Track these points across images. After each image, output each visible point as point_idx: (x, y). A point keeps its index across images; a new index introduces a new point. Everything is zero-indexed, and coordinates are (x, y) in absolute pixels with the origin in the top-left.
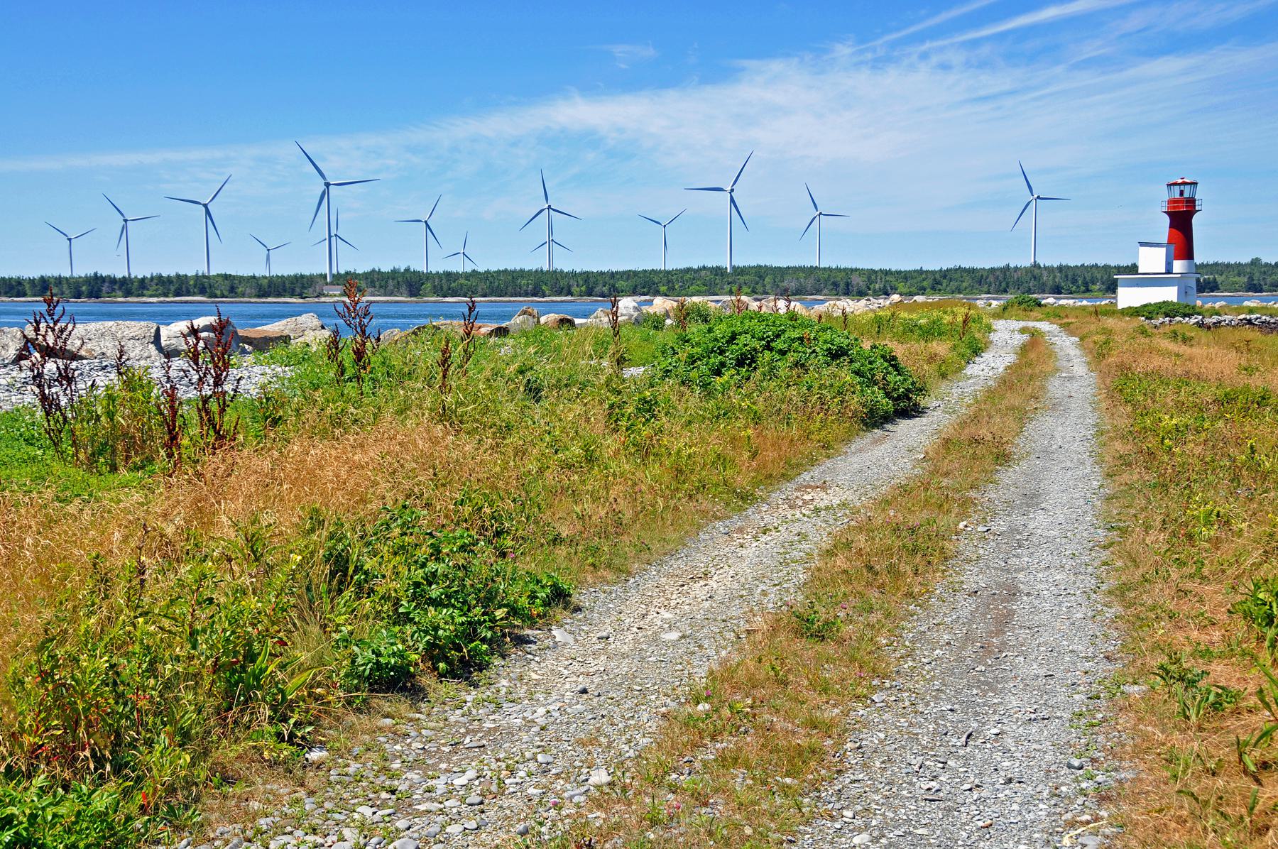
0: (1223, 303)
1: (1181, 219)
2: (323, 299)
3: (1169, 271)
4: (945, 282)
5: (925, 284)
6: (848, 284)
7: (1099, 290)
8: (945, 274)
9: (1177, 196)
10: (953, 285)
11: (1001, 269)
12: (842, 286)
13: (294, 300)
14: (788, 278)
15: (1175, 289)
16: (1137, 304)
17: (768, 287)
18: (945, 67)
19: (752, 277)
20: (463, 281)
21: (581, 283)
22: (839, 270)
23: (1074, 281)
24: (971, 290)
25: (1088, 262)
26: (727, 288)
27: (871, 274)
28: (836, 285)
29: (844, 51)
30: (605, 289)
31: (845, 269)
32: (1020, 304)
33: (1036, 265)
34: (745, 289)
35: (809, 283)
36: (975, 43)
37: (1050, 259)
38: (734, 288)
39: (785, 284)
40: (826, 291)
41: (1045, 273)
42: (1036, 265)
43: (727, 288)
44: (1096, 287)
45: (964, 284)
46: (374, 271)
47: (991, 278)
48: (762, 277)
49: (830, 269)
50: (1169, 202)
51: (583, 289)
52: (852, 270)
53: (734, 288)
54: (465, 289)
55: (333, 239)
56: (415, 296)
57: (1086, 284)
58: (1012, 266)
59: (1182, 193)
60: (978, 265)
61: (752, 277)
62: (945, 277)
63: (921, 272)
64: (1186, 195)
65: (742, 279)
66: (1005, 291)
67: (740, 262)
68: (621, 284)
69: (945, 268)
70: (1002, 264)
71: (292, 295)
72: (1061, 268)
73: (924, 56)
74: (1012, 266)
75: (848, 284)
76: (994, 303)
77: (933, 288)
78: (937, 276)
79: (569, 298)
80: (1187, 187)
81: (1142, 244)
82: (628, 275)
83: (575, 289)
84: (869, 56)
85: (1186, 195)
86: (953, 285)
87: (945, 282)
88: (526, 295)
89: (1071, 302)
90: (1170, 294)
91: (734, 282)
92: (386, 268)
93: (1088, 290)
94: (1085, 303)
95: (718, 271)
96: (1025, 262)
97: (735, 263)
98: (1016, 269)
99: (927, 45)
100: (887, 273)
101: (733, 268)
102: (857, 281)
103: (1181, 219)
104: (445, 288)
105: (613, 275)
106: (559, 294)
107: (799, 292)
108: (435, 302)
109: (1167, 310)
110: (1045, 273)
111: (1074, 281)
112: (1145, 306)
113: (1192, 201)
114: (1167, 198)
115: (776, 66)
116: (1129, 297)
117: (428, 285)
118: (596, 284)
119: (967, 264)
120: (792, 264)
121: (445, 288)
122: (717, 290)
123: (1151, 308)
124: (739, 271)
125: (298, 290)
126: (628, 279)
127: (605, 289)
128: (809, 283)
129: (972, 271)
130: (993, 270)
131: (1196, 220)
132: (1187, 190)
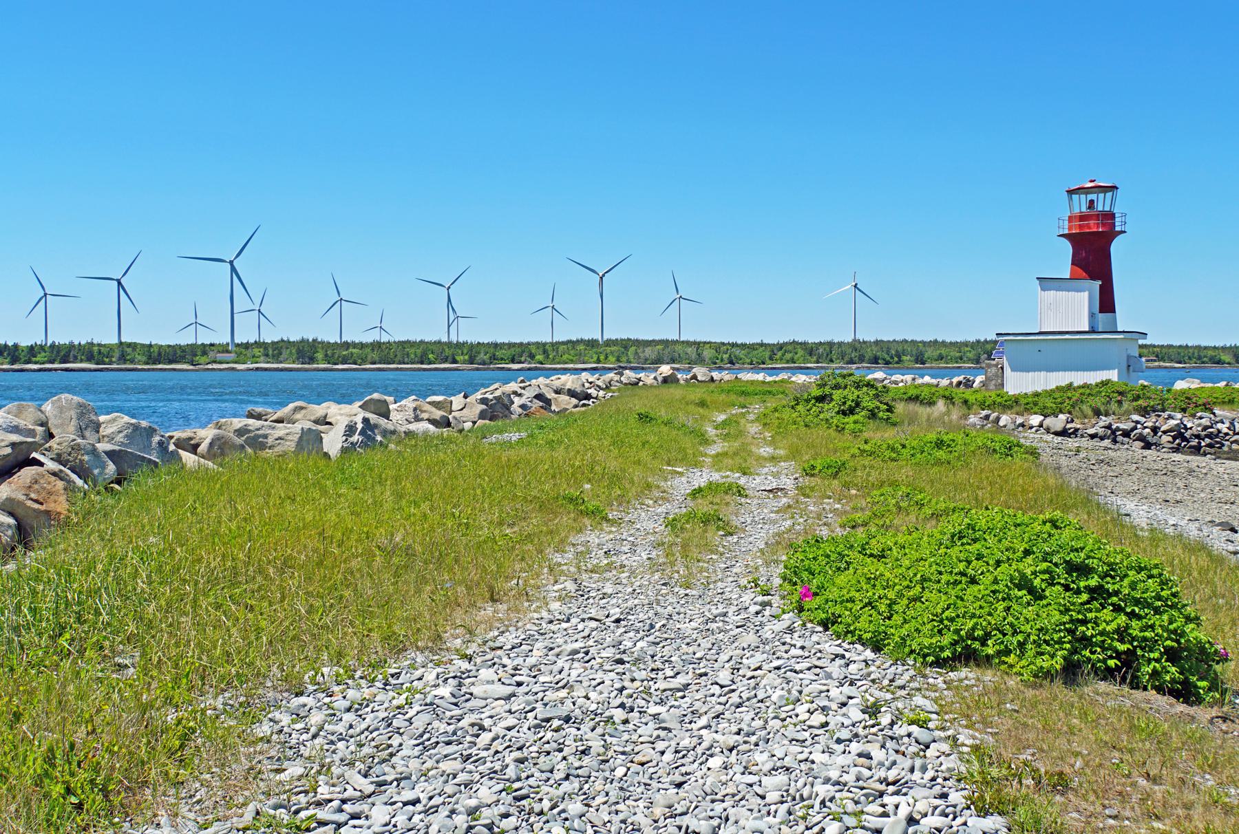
1: (1092, 251)
30: (486, 358)
48: (626, 348)
53: (602, 357)
72: (877, 342)
74: (76, 343)
80: (1101, 196)
94: (927, 379)
96: (848, 339)
97: (237, 341)
100: (734, 345)
101: (238, 345)
103: (1092, 251)
127: (486, 358)
129: (804, 344)
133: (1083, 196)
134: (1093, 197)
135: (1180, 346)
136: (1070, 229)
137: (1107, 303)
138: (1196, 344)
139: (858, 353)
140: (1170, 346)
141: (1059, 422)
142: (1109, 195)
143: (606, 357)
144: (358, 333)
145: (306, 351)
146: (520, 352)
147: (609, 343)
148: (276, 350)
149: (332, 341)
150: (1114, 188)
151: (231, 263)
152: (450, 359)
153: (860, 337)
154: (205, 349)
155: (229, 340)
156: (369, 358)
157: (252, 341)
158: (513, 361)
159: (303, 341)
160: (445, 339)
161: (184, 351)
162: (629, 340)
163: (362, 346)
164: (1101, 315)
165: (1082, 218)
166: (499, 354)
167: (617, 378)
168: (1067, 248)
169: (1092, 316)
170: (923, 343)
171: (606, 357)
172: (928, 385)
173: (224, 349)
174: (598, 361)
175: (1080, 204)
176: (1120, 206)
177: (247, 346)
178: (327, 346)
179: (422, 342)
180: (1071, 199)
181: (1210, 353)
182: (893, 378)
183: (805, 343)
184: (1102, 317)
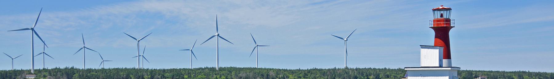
1: (442, 33)
5: (301, 75)
9: (439, 17)
11: (332, 69)
14: (242, 72)
19: (226, 72)
20: (94, 73)
21: (149, 74)
22: (265, 69)
25: (494, 70)
31: (268, 69)
33: (347, 68)
39: (240, 75)
41: (350, 71)
42: (347, 68)
45: (317, 75)
47: (328, 73)
48: (230, 72)
49: (261, 69)
50: (434, 21)
55: (141, 58)
58: (337, 68)
59: (442, 16)
60: (323, 68)
61: (226, 72)
62: (309, 72)
63: (300, 70)
64: (445, 17)
65: (222, 72)
69: (309, 69)
70: (333, 67)
72: (357, 69)
74: (337, 68)
78: (306, 72)
80: (445, 12)
81: (423, 47)
85: (445, 17)
87: (309, 75)
91: (218, 74)
92: (62, 67)
96: (343, 67)
97: (35, 68)
98: (339, 69)
101: (35, 70)
103: (442, 33)
105: (164, 70)
110: (350, 71)
113: (448, 20)
118: (155, 74)
119: (319, 68)
126: (171, 72)
130: (329, 70)
131: (451, 33)
132: (445, 14)
133: (439, 12)
134: (442, 12)
135: (489, 71)
136: (434, 25)
137: (447, 55)
140: (492, 72)
142: (448, 11)
147: (221, 69)
149: (81, 68)
150: (450, 9)
151: (32, 29)
153: (349, 66)
155: (32, 68)
157: (42, 68)
159: (66, 68)
160: (137, 67)
161: (10, 73)
162: (231, 67)
166: (166, 75)
168: (433, 33)
170: (379, 69)
175: (438, 15)
176: (453, 16)
177: (39, 71)
179: (126, 69)
180: (434, 13)
181: (509, 74)
184: (445, 61)
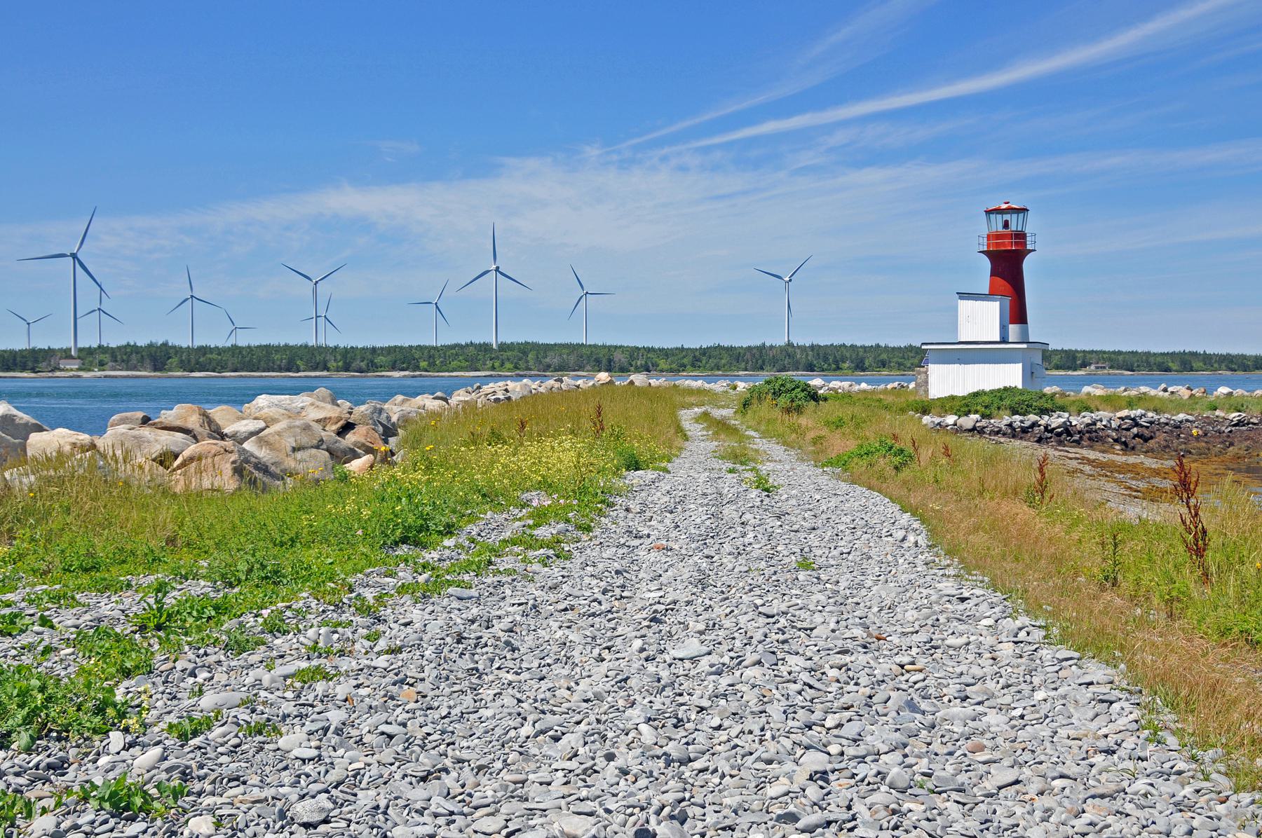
0: (1055, 389)
1: (1007, 264)
2: (58, 374)
3: (1004, 340)
4: (704, 359)
5: (685, 361)
6: (610, 361)
7: (849, 368)
8: (704, 352)
9: (1000, 229)
10: (712, 362)
12: (604, 361)
13: (24, 374)
15: (1018, 368)
16: (961, 391)
17: (531, 363)
18: (683, 169)
20: (214, 356)
22: (604, 347)
23: (826, 359)
24: (729, 366)
26: (489, 363)
27: (634, 352)
28: (598, 361)
29: (592, 152)
30: (363, 365)
31: (610, 347)
32: (777, 394)
33: (790, 344)
34: (508, 365)
35: (572, 359)
36: (707, 150)
37: (802, 339)
38: (497, 364)
39: (548, 360)
40: (588, 367)
41: (798, 351)
42: (790, 344)
43: (489, 363)
44: (846, 365)
46: (128, 345)
47: (748, 356)
48: (525, 353)
49: (595, 346)
51: (340, 364)
52: (616, 347)
53: (497, 364)
54: (214, 364)
56: (160, 370)
57: (836, 362)
58: (768, 344)
59: (1006, 225)
61: (515, 353)
62: (704, 354)
63: (682, 349)
64: (1013, 227)
66: (762, 369)
67: (508, 338)
68: (379, 360)
70: (758, 343)
71: (23, 369)
72: (812, 347)
73: (664, 159)
74: (768, 344)
75: (610, 361)
76: (741, 386)
77: (693, 365)
79: (325, 373)
80: (1014, 216)
81: (964, 296)
82: (390, 350)
83: (332, 364)
84: (615, 157)
85: (1013, 227)
86: (712, 362)
87: (704, 359)
88: (280, 370)
89: (846, 384)
90: (1010, 376)
91: (497, 358)
93: (838, 368)
94: (864, 386)
95: (485, 348)
96: (781, 341)
97: (80, 345)
98: (771, 347)
99: (666, 150)
100: (649, 350)
101: (81, 350)
102: (619, 357)
103: (1007, 264)
104: (193, 362)
106: (315, 369)
107: (562, 368)
108: (179, 377)
109: (1000, 399)
110: (798, 351)
111: (826, 359)
112: (976, 394)
113: (1021, 236)
114: (985, 232)
115: (532, 163)
116: (945, 381)
117: (174, 361)
119: (726, 344)
120: (559, 342)
121: (193, 362)
122: (479, 365)
123: (987, 399)
124: (503, 347)
125: (30, 364)
127: (363, 365)
128: (572, 359)
129: (730, 349)
130: (749, 348)
131: (1028, 264)
133: (999, 216)
134: (1007, 217)
135: (1114, 352)
136: (988, 245)
137: (1018, 314)
138: (1146, 350)
139: (788, 357)
140: (1120, 353)
141: (970, 421)
142: (1021, 215)
143: (502, 364)
144: (218, 339)
145: (159, 357)
146: (404, 358)
148: (127, 356)
149: (184, 346)
150: (1024, 210)
151: (74, 256)
152: (321, 366)
153: (796, 341)
154: (49, 353)
155: (72, 344)
156: (230, 364)
158: (393, 368)
160: (312, 343)
161: (23, 357)
162: (527, 343)
163: (219, 351)
164: (1011, 326)
165: (999, 236)
167: (557, 385)
168: (986, 264)
169: (1004, 329)
170: (864, 347)
171: (502, 364)
172: (864, 391)
173: (66, 354)
174: (493, 368)
175: (997, 224)
176: (1031, 226)
177: (90, 351)
178: (178, 350)
180: (989, 220)
181: (1159, 359)
182: (831, 385)
183: (731, 349)
184: (1013, 329)
